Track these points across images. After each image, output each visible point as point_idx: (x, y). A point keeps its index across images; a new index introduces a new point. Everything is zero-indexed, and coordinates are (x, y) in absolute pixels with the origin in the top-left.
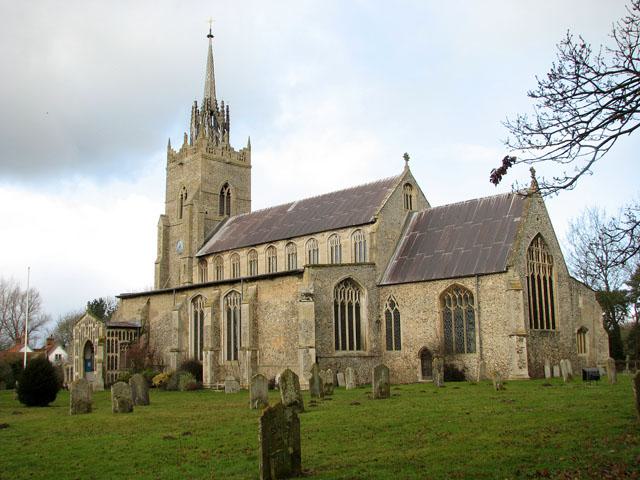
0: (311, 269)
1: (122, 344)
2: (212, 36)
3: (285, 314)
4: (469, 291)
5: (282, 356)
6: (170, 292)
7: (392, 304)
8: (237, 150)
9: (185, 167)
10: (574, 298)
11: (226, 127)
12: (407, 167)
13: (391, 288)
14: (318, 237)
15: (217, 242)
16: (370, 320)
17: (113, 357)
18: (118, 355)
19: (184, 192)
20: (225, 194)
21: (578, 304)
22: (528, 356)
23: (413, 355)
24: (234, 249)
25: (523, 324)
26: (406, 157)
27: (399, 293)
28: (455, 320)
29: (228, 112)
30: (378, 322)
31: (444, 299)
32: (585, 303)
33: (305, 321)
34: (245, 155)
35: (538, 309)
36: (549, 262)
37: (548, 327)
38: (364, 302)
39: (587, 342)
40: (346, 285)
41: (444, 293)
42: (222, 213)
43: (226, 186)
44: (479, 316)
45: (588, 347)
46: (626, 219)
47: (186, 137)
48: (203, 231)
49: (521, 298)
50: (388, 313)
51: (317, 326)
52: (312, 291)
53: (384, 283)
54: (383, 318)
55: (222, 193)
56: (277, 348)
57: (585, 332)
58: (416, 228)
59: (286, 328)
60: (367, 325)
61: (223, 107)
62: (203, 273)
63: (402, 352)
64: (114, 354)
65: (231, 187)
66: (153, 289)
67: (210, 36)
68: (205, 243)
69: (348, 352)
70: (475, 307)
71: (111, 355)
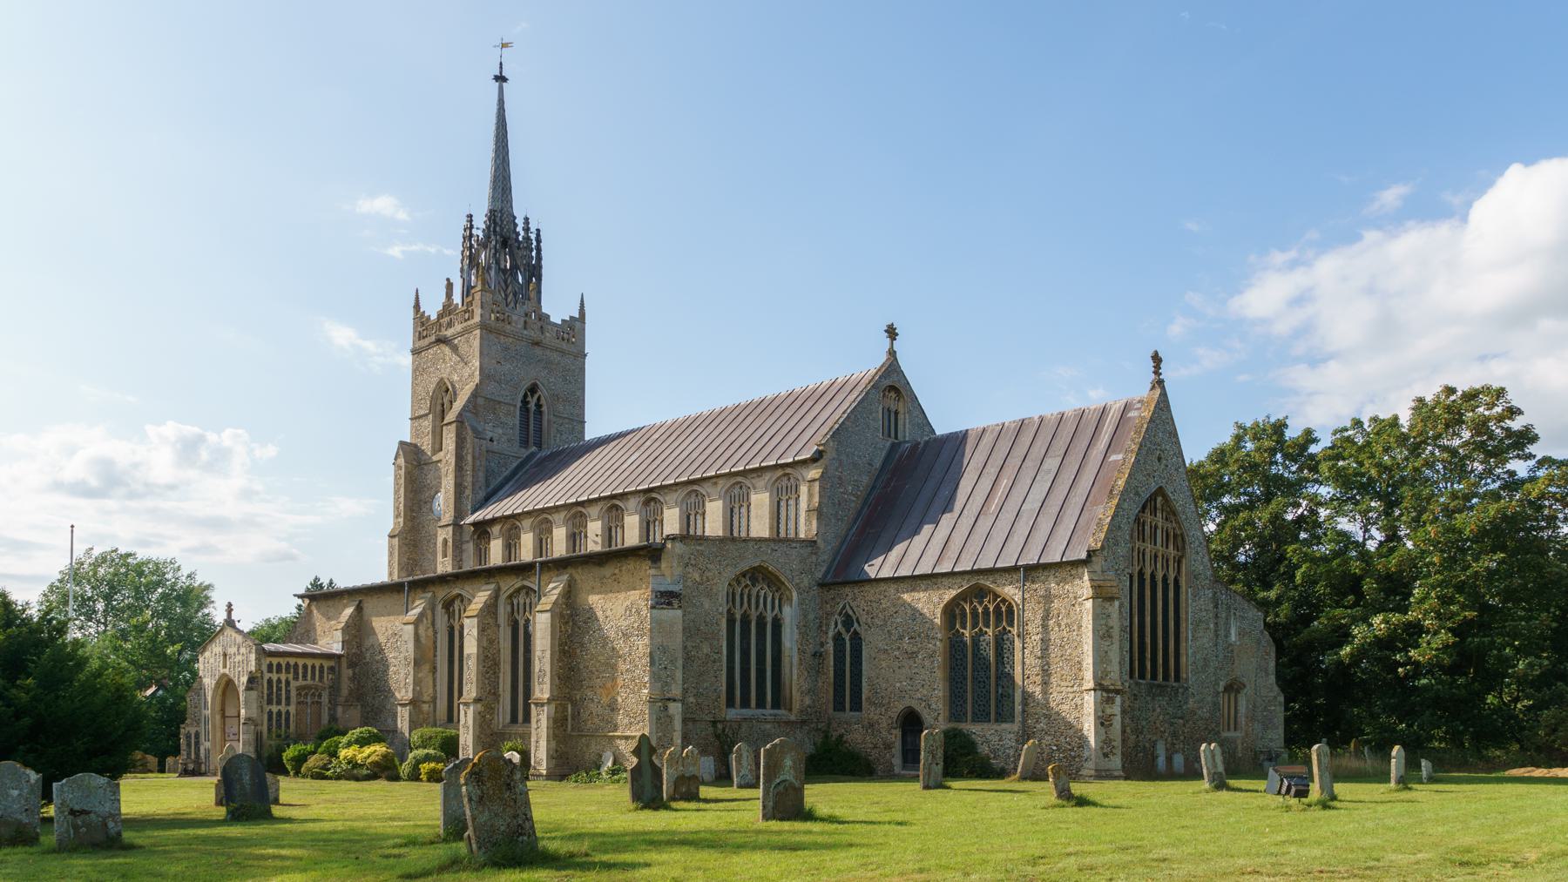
0: (678, 545)
1: (298, 689)
7: (848, 622)
8: (556, 319)
10: (1221, 622)
11: (535, 272)
12: (892, 353)
15: (1023, 764)
16: (801, 652)
17: (279, 713)
18: (292, 709)
20: (532, 406)
21: (1227, 635)
22: (1124, 732)
25: (1116, 668)
26: (892, 332)
29: (539, 240)
30: (818, 655)
32: (1241, 634)
34: (574, 328)
35: (1148, 640)
36: (1176, 548)
37: (1166, 677)
38: (789, 614)
39: (1242, 710)
40: (754, 581)
42: (525, 443)
45: (1242, 721)
47: (450, 286)
48: (481, 475)
49: (1115, 615)
50: (838, 638)
51: (688, 659)
52: (676, 588)
54: (830, 647)
55: (525, 402)
57: (1238, 691)
60: (795, 660)
61: (527, 229)
62: (482, 554)
64: (275, 709)
65: (543, 392)
69: (752, 711)
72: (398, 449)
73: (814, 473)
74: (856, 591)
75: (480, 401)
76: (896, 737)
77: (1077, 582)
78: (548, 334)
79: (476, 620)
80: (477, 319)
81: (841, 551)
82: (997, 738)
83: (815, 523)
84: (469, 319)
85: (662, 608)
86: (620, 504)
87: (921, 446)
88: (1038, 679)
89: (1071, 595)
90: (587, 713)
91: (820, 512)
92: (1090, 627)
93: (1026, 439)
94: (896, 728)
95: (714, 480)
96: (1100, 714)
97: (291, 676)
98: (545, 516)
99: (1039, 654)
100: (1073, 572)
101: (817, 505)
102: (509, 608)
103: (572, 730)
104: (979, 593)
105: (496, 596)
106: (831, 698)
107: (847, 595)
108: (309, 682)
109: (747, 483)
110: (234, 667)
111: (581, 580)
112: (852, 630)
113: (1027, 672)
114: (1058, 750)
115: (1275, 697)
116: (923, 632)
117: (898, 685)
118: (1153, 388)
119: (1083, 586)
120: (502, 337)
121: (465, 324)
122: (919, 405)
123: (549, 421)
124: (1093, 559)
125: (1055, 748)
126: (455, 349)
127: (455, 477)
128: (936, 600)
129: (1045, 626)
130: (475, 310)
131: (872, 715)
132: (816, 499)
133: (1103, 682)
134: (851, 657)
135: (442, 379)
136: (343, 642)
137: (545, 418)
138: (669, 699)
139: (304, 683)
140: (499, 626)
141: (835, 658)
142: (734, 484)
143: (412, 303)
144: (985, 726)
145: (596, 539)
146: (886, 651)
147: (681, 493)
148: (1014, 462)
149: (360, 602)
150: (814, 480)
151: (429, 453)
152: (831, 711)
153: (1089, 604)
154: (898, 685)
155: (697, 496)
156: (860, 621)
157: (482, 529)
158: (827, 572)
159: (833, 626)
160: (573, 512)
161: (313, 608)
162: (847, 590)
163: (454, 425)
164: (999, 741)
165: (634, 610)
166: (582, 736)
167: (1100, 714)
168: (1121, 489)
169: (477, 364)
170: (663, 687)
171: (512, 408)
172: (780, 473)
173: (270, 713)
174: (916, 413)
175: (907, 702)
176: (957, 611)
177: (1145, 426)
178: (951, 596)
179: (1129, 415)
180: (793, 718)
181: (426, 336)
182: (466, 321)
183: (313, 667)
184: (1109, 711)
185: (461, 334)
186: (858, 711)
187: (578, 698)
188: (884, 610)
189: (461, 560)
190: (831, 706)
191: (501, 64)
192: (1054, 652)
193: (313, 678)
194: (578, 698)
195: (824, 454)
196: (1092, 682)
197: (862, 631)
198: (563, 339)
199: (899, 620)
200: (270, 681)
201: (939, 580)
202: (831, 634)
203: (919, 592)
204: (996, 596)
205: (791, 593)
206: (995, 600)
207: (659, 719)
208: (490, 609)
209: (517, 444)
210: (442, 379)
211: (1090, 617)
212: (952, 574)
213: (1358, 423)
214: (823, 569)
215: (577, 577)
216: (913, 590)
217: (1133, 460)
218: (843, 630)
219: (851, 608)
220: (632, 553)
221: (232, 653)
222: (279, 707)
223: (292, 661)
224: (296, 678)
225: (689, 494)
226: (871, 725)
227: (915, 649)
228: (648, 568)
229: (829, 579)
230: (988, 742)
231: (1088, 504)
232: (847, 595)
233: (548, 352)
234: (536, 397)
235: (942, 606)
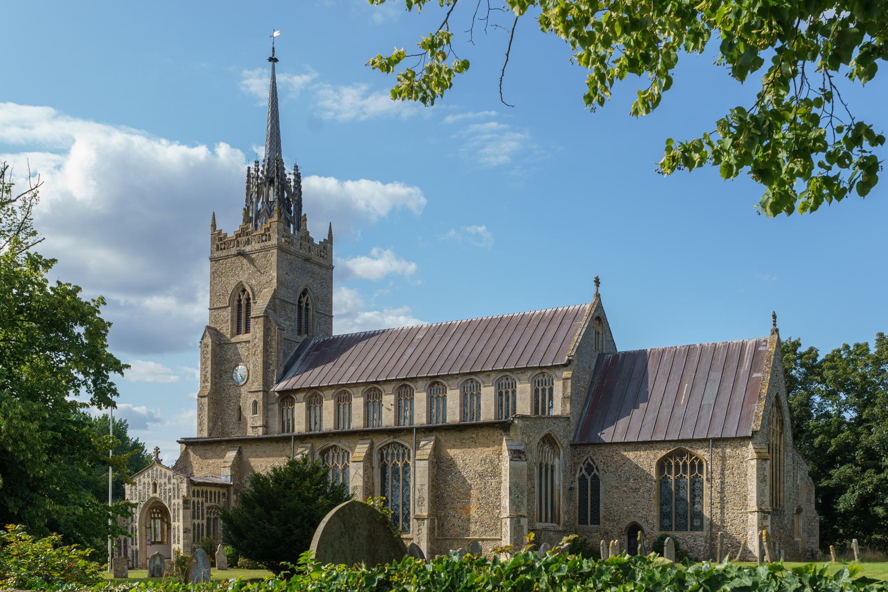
1: (208, 508)
2: (276, 60)
7: (590, 469)
12: (598, 296)
16: (564, 487)
17: (199, 524)
19: (243, 298)
20: (303, 304)
26: (597, 282)
42: (300, 332)
43: (14, 184)
50: (582, 479)
52: (521, 448)
54: (577, 485)
55: (300, 302)
65: (310, 295)
66: (196, 437)
67: (273, 60)
71: (196, 522)
72: (205, 330)
73: (567, 374)
74: (596, 450)
75: (277, 302)
76: (624, 540)
77: (744, 448)
78: (313, 253)
79: (362, 463)
80: (274, 241)
81: (581, 424)
82: (692, 540)
83: (568, 406)
84: (266, 241)
85: (517, 460)
86: (411, 385)
87: (620, 357)
88: (719, 505)
89: (740, 457)
90: (450, 525)
91: (570, 399)
92: (755, 476)
93: (543, 326)
94: (623, 535)
95: (488, 373)
96: (760, 525)
97: (204, 499)
98: (344, 389)
99: (719, 490)
100: (742, 443)
101: (570, 394)
103: (438, 535)
104: (681, 453)
105: (371, 448)
106: (577, 516)
107: (589, 452)
108: (213, 504)
109: (514, 376)
110: (165, 493)
111: (445, 440)
112: (593, 473)
113: (713, 501)
114: (731, 547)
115: (815, 517)
116: (643, 476)
117: (626, 508)
118: (773, 334)
119: (750, 451)
120: (289, 255)
121: (262, 244)
122: (609, 328)
123: (313, 315)
124: (755, 436)
125: (730, 545)
126: (252, 261)
127: (263, 356)
128: (652, 457)
129: (723, 474)
130: (272, 235)
131: (607, 527)
132: (569, 391)
133: (762, 507)
134: (591, 491)
135: (240, 284)
136: (231, 476)
137: (311, 313)
138: (521, 516)
139: (211, 504)
140: (373, 468)
141: (579, 491)
142: (502, 377)
143: (210, 222)
144: (685, 533)
145: (390, 407)
147: (460, 380)
148: (690, 374)
149: (240, 447)
150: (568, 379)
151: (229, 336)
152: (577, 524)
153: (754, 462)
154: (626, 508)
155: (472, 382)
156: (599, 468)
157: (287, 397)
158: (575, 437)
159: (579, 471)
160: (369, 387)
161: (190, 451)
162: (589, 448)
163: (263, 318)
164: (694, 542)
165: (488, 460)
166: (446, 539)
167: (760, 525)
168: (765, 395)
169: (275, 274)
170: (516, 509)
171: (294, 307)
172: (539, 371)
173: (194, 525)
174: (608, 333)
175: (632, 519)
176: (666, 464)
177: (773, 357)
178: (663, 455)
179: (760, 349)
180: (561, 529)
181: (224, 249)
182: (263, 241)
183: (211, 492)
184: (765, 524)
185: (259, 251)
186: (596, 524)
187: (442, 515)
188: (616, 462)
189: (267, 416)
190: (577, 521)
191: (273, 49)
192: (729, 490)
193: (215, 502)
194: (442, 515)
195: (571, 362)
196: (756, 507)
198: (321, 256)
199: (626, 469)
200: (194, 502)
201: (654, 445)
202: (577, 476)
203: (640, 451)
204: (692, 456)
205: (559, 450)
206: (691, 458)
207: (515, 528)
208: (369, 456)
209: (296, 333)
210: (240, 284)
211: (755, 470)
212: (664, 441)
213: (847, 347)
214: (572, 435)
215: (441, 438)
216: (636, 450)
217: (769, 377)
218: (586, 474)
219: (592, 460)
221: (163, 483)
222: (199, 521)
223: (205, 488)
224: (206, 501)
225: (467, 381)
226: (606, 533)
227: (637, 486)
228: (499, 434)
229: (577, 441)
230: (686, 542)
231: (745, 403)
232: (589, 452)
233: (313, 266)
234: (306, 298)
235: (656, 460)
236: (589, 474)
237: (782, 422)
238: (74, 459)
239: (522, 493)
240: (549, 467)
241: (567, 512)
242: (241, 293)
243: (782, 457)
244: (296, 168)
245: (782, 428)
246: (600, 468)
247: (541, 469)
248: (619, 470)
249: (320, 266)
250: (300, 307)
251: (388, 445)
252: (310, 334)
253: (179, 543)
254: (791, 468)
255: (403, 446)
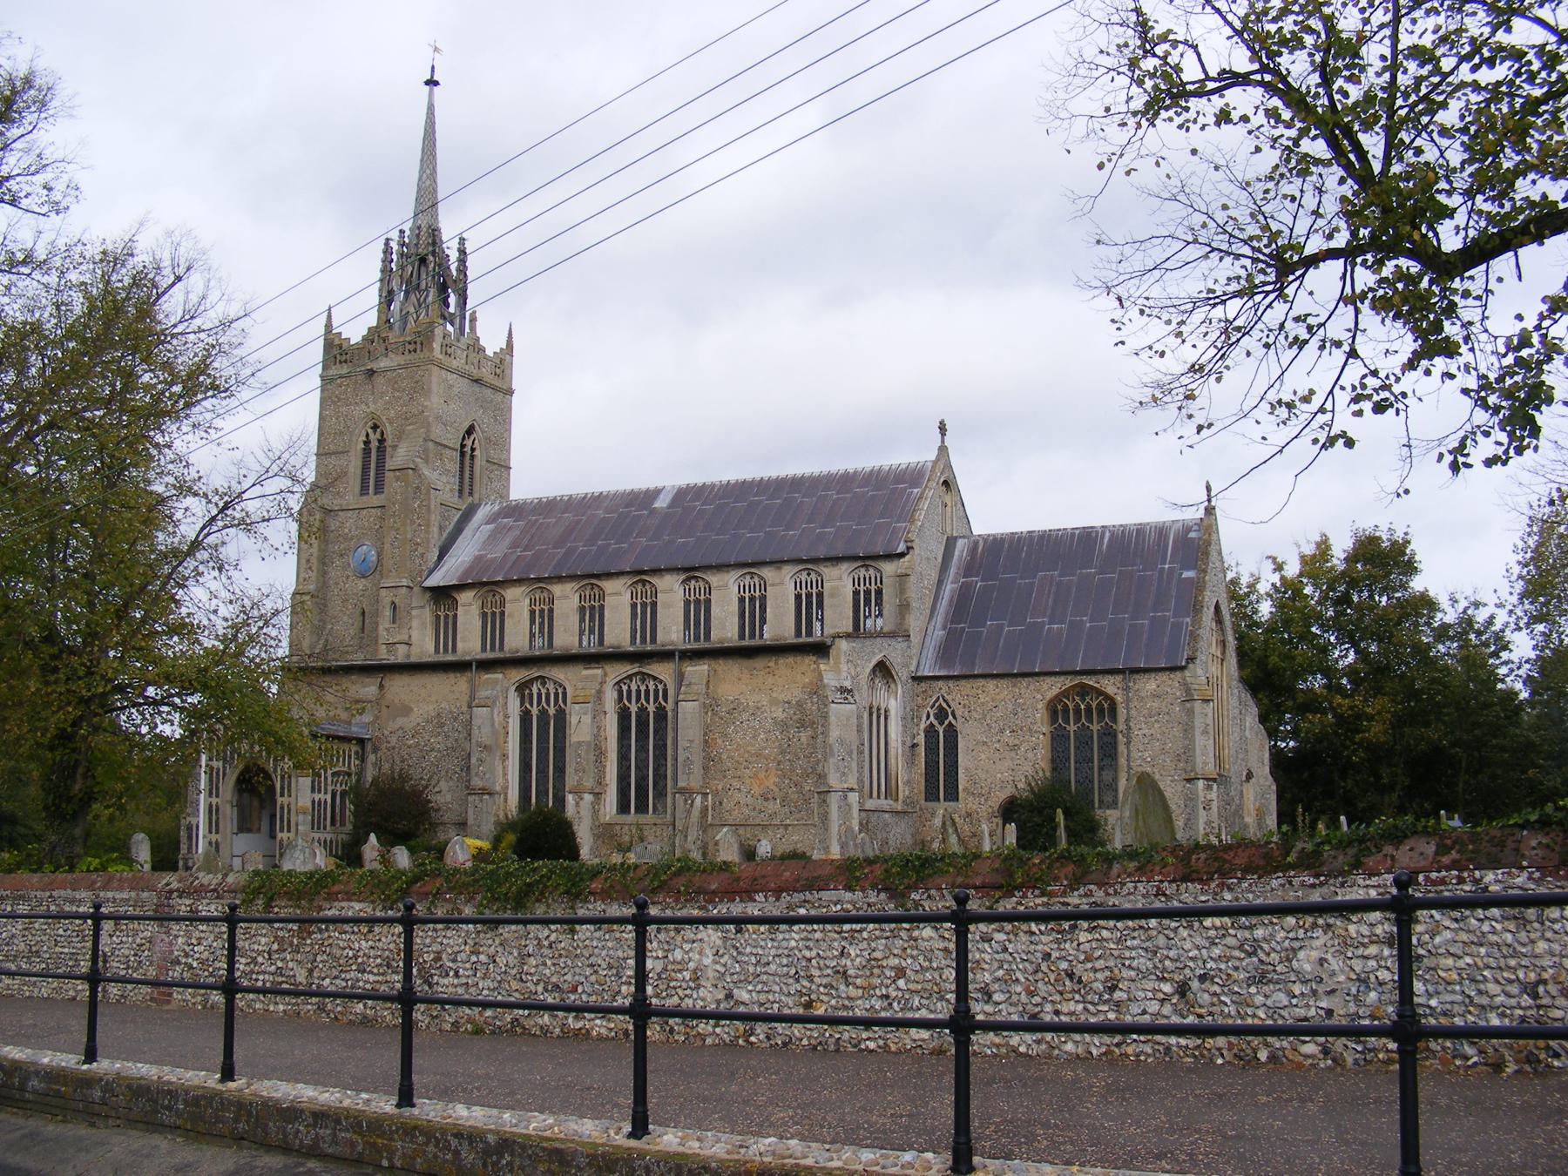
2: (436, 83)
3: (784, 726)
4: (1108, 697)
5: (773, 806)
6: (461, 667)
7: (941, 714)
9: (379, 380)
12: (943, 450)
13: (940, 683)
14: (768, 573)
16: (904, 743)
19: (374, 438)
20: (468, 449)
23: (984, 811)
24: (539, 580)
26: (943, 429)
27: (957, 696)
28: (1077, 748)
31: (1056, 710)
33: (842, 742)
41: (1057, 699)
44: (1128, 744)
46: (228, 552)
50: (931, 732)
52: (848, 684)
53: (926, 674)
54: (921, 739)
55: (463, 446)
56: (756, 790)
58: (969, 569)
59: (783, 752)
62: (446, 628)
63: (961, 805)
67: (432, 83)
68: (441, 557)
70: (1121, 726)
71: (317, 797)
102: (615, 694)
106: (923, 788)
112: (946, 722)
121: (408, 357)
137: (478, 462)
146: (985, 743)
159: (924, 718)
180: (899, 808)
184: (1208, 797)
187: (720, 787)
191: (433, 67)
194: (720, 787)
197: (959, 726)
202: (923, 726)
218: (936, 723)
220: (779, 650)
227: (1017, 742)
236: (941, 723)
237: (1223, 643)
238: (1168, 957)
239: (850, 753)
240: (882, 712)
241: (908, 782)
242: (370, 431)
243: (1225, 697)
244: (462, 241)
245: (1223, 653)
246: (958, 713)
247: (871, 715)
248: (988, 717)
249: (495, 389)
250: (463, 454)
251: (630, 677)
252: (476, 495)
253: (289, 831)
254: (1236, 711)
255: (655, 678)
